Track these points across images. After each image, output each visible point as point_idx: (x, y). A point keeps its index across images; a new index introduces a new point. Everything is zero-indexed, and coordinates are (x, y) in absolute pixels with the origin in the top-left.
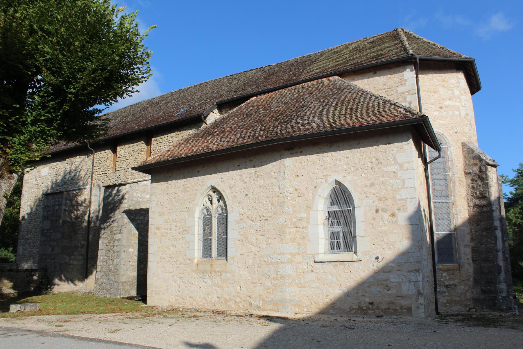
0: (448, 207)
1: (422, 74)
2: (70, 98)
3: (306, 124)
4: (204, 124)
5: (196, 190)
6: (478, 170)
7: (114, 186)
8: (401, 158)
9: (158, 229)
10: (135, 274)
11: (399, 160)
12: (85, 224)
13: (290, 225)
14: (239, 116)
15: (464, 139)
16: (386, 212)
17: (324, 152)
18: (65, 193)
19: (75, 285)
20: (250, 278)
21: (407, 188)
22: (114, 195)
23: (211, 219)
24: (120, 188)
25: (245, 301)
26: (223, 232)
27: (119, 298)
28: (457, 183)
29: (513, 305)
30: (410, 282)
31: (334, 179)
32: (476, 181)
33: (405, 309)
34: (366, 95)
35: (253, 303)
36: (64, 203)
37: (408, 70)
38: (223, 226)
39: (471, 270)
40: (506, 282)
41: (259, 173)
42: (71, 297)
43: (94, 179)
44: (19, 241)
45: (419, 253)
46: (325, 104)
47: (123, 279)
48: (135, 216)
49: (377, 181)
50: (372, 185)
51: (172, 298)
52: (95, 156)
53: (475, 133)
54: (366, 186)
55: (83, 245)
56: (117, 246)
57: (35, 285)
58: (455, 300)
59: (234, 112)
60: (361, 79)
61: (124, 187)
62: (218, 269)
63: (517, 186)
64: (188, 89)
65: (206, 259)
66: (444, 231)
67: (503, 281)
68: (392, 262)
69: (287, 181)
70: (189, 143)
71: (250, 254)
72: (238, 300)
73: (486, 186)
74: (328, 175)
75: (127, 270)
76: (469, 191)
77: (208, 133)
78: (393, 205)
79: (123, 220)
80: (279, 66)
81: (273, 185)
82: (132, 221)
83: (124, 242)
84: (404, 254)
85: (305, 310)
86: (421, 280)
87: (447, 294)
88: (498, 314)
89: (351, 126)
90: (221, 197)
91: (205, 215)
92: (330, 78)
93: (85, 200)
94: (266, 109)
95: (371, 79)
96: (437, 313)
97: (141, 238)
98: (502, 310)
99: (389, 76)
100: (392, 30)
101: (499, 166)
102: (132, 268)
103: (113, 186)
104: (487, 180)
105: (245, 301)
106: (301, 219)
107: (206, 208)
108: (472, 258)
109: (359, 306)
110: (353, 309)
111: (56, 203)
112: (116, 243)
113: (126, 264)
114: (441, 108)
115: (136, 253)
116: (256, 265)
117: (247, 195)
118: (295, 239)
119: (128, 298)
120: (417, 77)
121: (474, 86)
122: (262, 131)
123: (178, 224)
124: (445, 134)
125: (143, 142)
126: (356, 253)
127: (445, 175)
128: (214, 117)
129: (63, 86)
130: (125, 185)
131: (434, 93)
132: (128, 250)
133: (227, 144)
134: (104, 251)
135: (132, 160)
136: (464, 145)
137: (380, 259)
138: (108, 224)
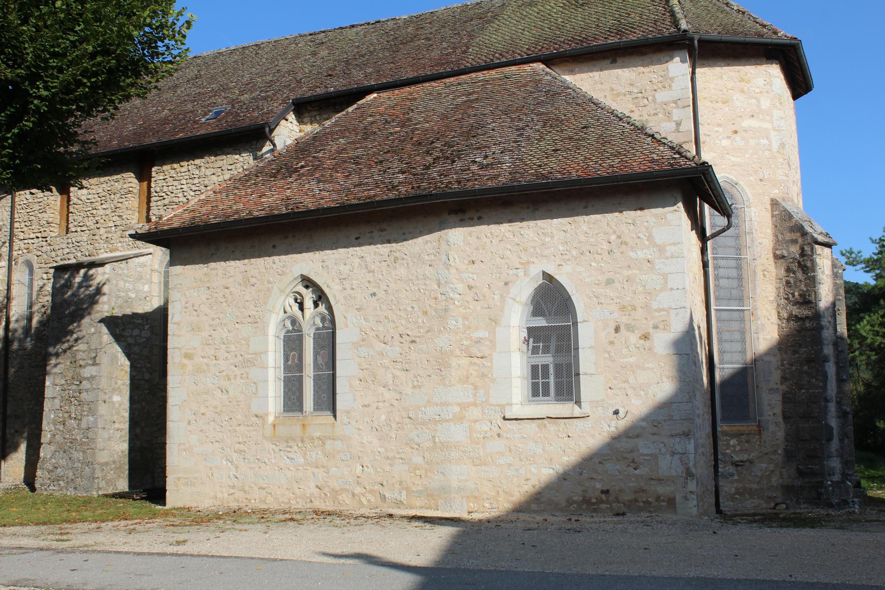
0: (741, 318)
1: (703, 66)
2: (36, 106)
3: (488, 165)
4: (268, 143)
6: (799, 251)
8: (661, 236)
9: (188, 356)
10: (125, 446)
11: (658, 240)
13: (458, 352)
14: (347, 134)
15: (776, 193)
16: (633, 332)
20: (382, 450)
21: (672, 289)
22: (76, 285)
23: (300, 339)
24: (91, 272)
25: (371, 492)
26: (326, 364)
27: (96, 496)
29: (851, 496)
30: (673, 454)
31: (541, 270)
32: (794, 273)
33: (663, 501)
34: (599, 110)
35: (387, 495)
37: (677, 59)
38: (326, 352)
39: (781, 435)
41: (397, 254)
43: (15, 247)
45: (690, 404)
46: (521, 125)
48: (123, 330)
49: (618, 276)
50: (609, 282)
51: (222, 492)
52: (17, 199)
54: (598, 284)
56: (87, 391)
58: (751, 489)
59: (335, 124)
60: (586, 72)
61: (100, 269)
62: (318, 434)
63: (878, 272)
64: (215, 57)
65: (291, 414)
66: (732, 363)
67: (835, 453)
68: (644, 419)
69: (453, 271)
70: (249, 187)
71: (381, 405)
72: (358, 490)
73: (812, 281)
74: (529, 262)
75: (109, 439)
76: (782, 290)
77: (286, 167)
78: (646, 319)
79: (101, 337)
80: (417, 21)
81: (425, 277)
82: (118, 338)
83: (103, 383)
85: (487, 505)
86: (693, 451)
87: (736, 477)
88: (823, 512)
89: (574, 175)
90: (321, 297)
91: (288, 332)
92: (527, 67)
95: (606, 72)
96: (719, 511)
97: (134, 373)
98: (831, 506)
99: (641, 69)
101: (835, 244)
102: (118, 434)
103: (76, 268)
104: (814, 271)
105: (371, 492)
106: (478, 341)
107: (290, 317)
108: (783, 412)
109: (584, 497)
112: (85, 384)
113: (107, 427)
114: (736, 132)
115: (127, 404)
116: (394, 426)
117: (374, 294)
118: (468, 378)
120: (693, 73)
121: (799, 83)
122: (403, 173)
124: (741, 183)
125: (133, 175)
126: (578, 402)
127: (737, 259)
128: (288, 132)
129: (23, 83)
130: (102, 264)
131: (724, 103)
132: (110, 398)
133: (335, 196)
134: (57, 401)
135: (108, 212)
136: (774, 203)
138: (66, 345)
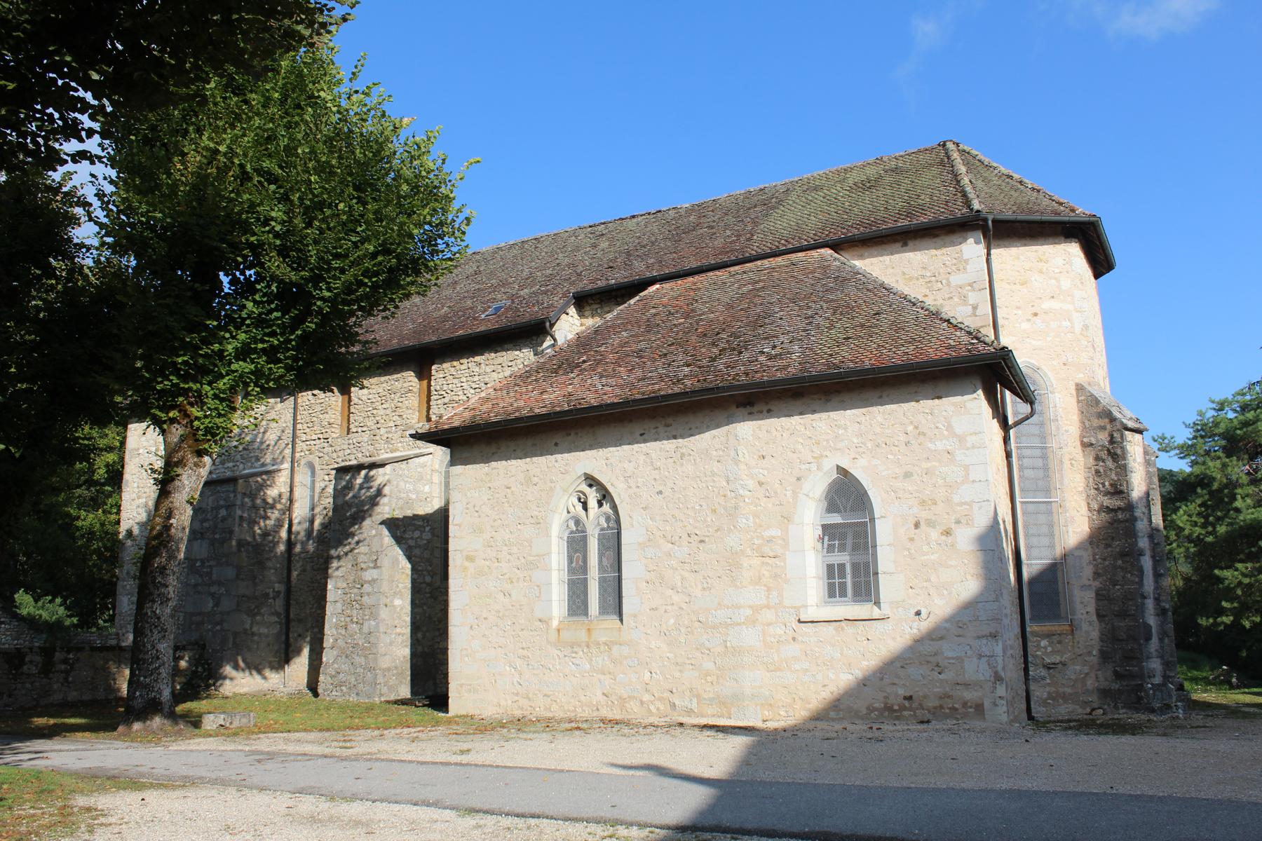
1: (999, 246)
4: (549, 338)
5: (552, 481)
6: (1108, 438)
7: (360, 467)
9: (470, 558)
10: (407, 652)
11: (958, 431)
12: (282, 547)
13: (749, 552)
15: (1081, 378)
16: (934, 527)
17: (814, 412)
18: (241, 481)
19: (265, 678)
24: (372, 473)
25: (661, 699)
28: (1067, 464)
30: (980, 656)
36: (238, 502)
37: (971, 240)
38: (611, 554)
39: (1095, 634)
40: (1162, 657)
41: (684, 450)
42: (261, 700)
43: (298, 449)
44: (120, 583)
47: (385, 663)
50: (907, 475)
52: (299, 400)
53: (1104, 359)
55: (279, 592)
56: (368, 594)
57: (183, 680)
59: (617, 317)
61: (381, 470)
65: (575, 618)
67: (1154, 654)
69: (742, 467)
70: (530, 383)
71: (669, 608)
72: (646, 697)
73: (1123, 470)
75: (391, 644)
77: (567, 362)
79: (382, 539)
80: (700, 210)
81: (713, 474)
82: (399, 540)
83: (385, 587)
84: (970, 606)
85: (782, 713)
86: (1001, 654)
90: (605, 496)
91: (572, 532)
93: (280, 496)
94: (687, 316)
95: (897, 256)
96: (1030, 717)
98: (1153, 711)
99: (934, 252)
100: (935, 144)
102: (400, 639)
104: (1124, 459)
105: (661, 699)
106: (770, 540)
108: (1097, 610)
109: (886, 704)
110: (876, 709)
111: (222, 503)
112: (367, 588)
114: (1036, 314)
116: (683, 630)
117: (661, 492)
119: (396, 702)
120: (989, 254)
121: (1100, 262)
122: (688, 366)
123: (515, 550)
126: (877, 603)
127: (1042, 448)
128: (569, 326)
130: (383, 465)
132: (392, 601)
133: (618, 391)
134: (339, 605)
135: (388, 412)
136: (1080, 388)
137: (924, 615)
138: (347, 548)
